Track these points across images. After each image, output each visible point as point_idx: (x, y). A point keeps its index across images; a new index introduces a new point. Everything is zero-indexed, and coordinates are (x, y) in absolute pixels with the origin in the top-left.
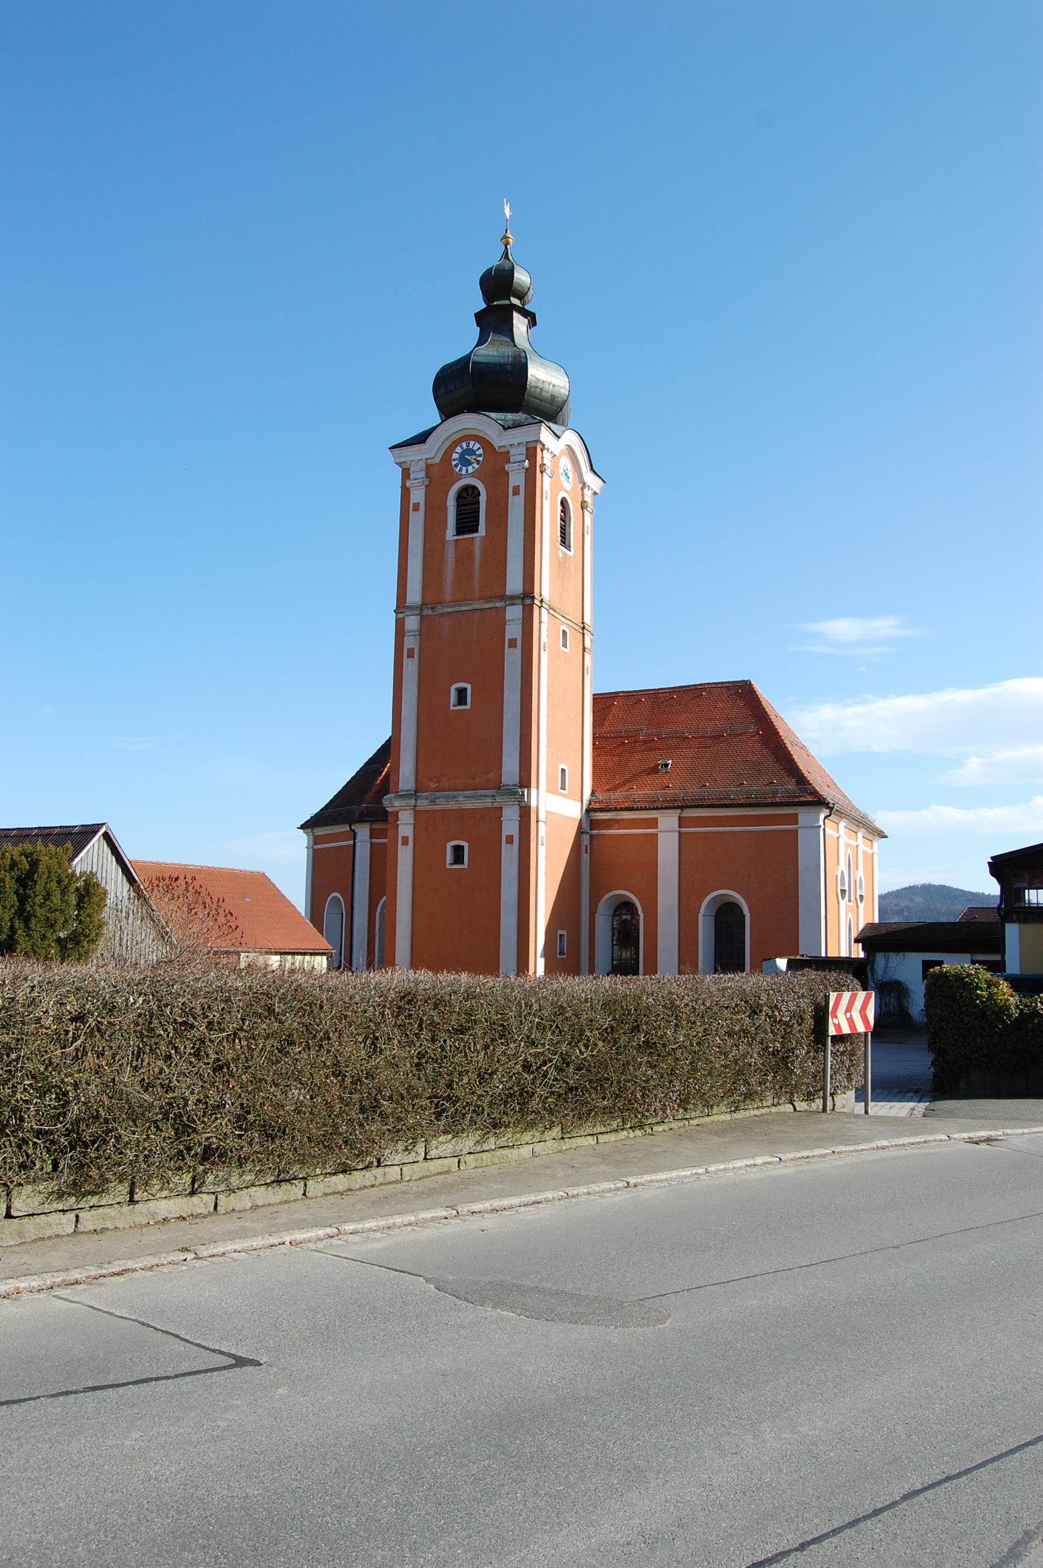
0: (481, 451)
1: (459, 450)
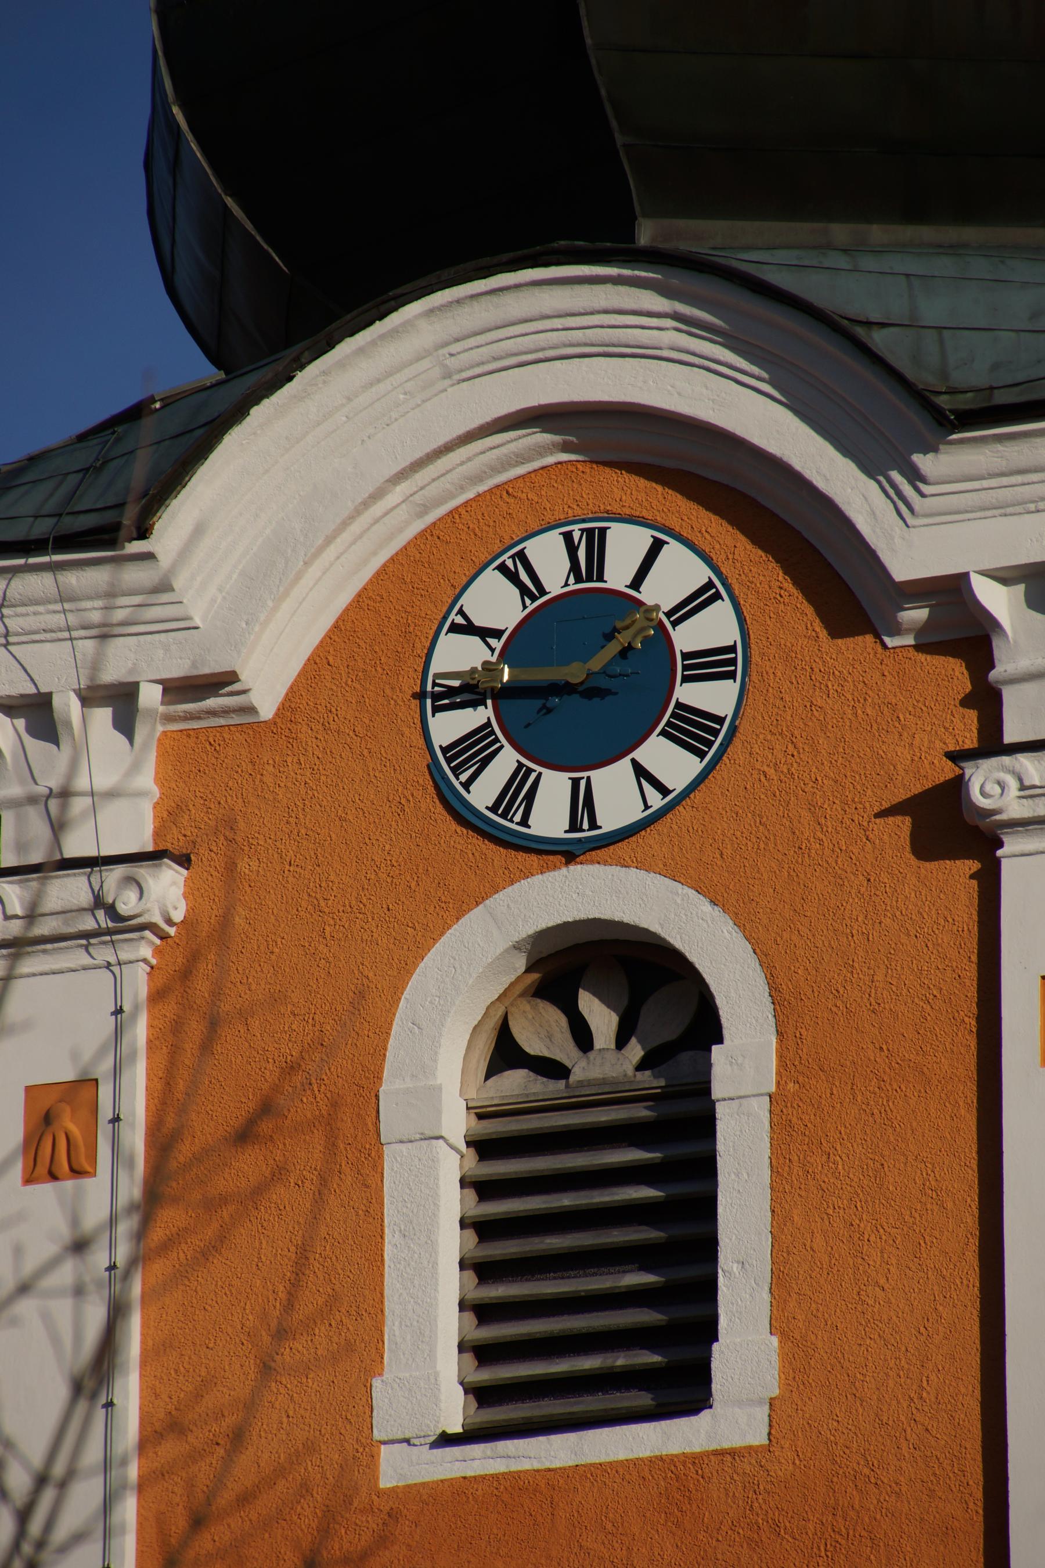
0: (714, 628)
1: (495, 602)
